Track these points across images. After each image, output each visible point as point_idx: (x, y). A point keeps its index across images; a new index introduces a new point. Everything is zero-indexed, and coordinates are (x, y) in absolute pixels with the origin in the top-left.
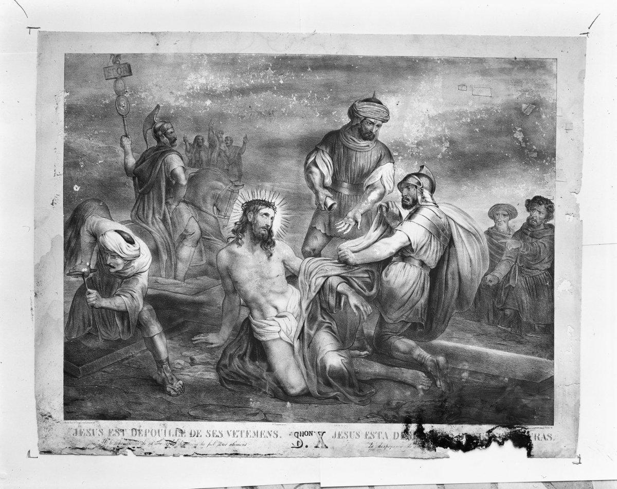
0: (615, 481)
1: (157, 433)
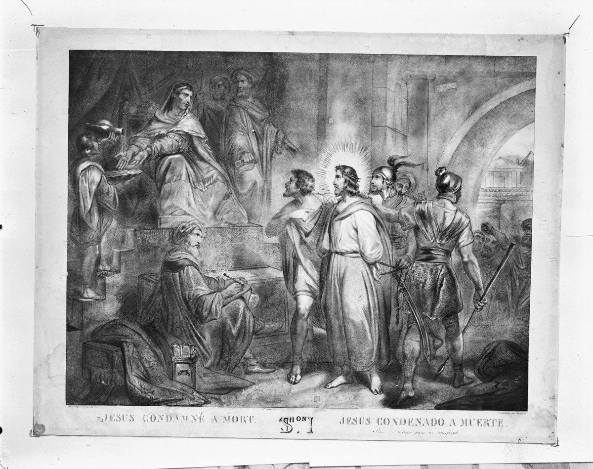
0: (591, 464)
1: (437, 423)
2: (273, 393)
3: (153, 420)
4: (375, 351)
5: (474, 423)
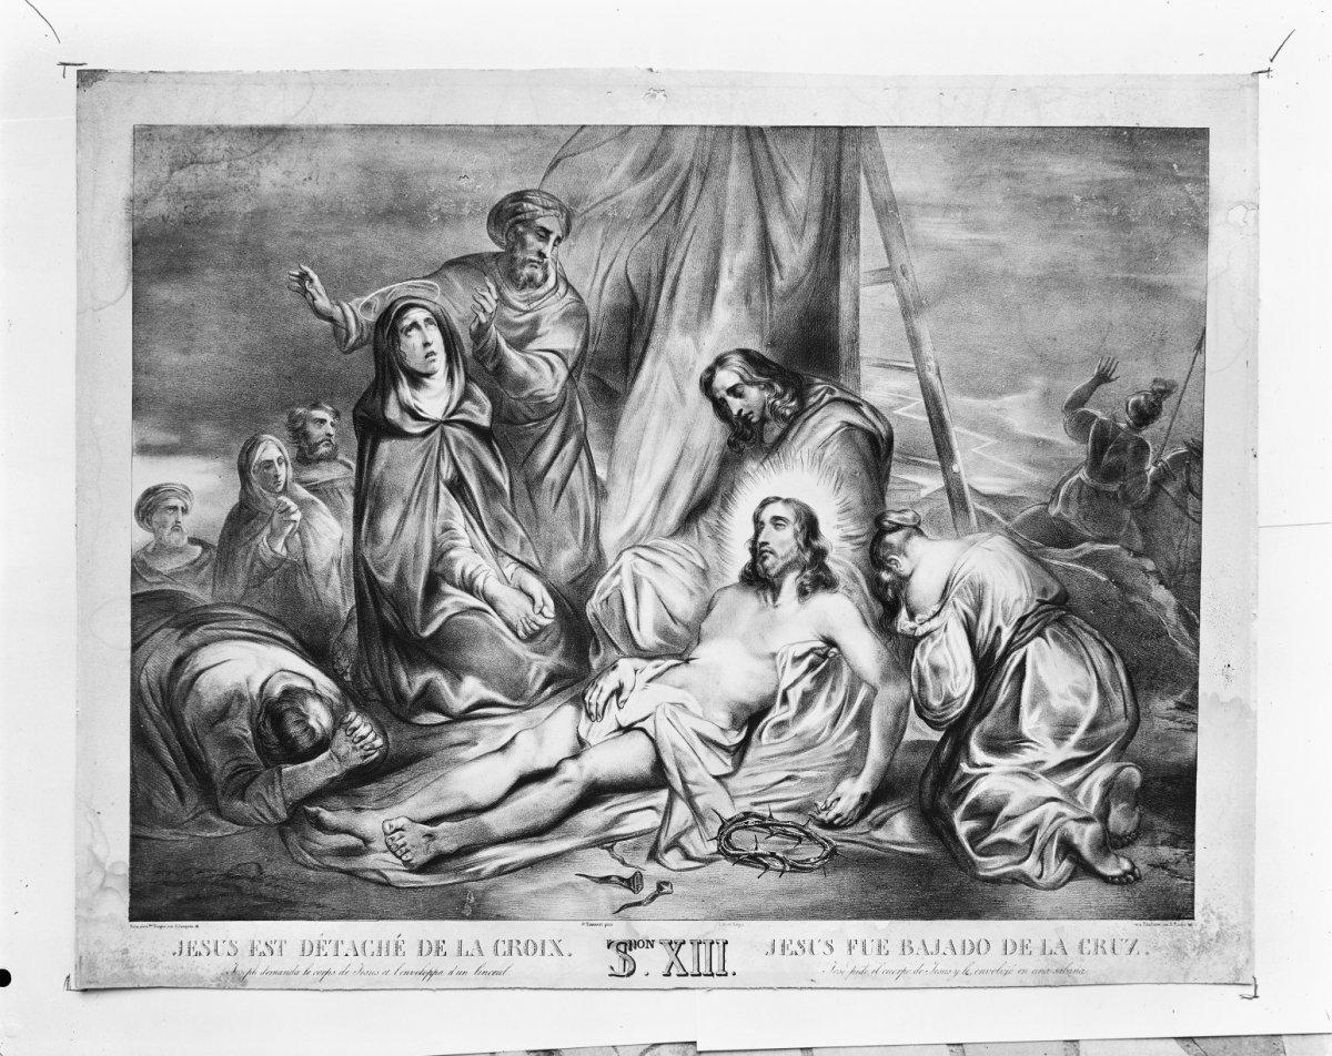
2: (991, 794)
5: (488, 947)
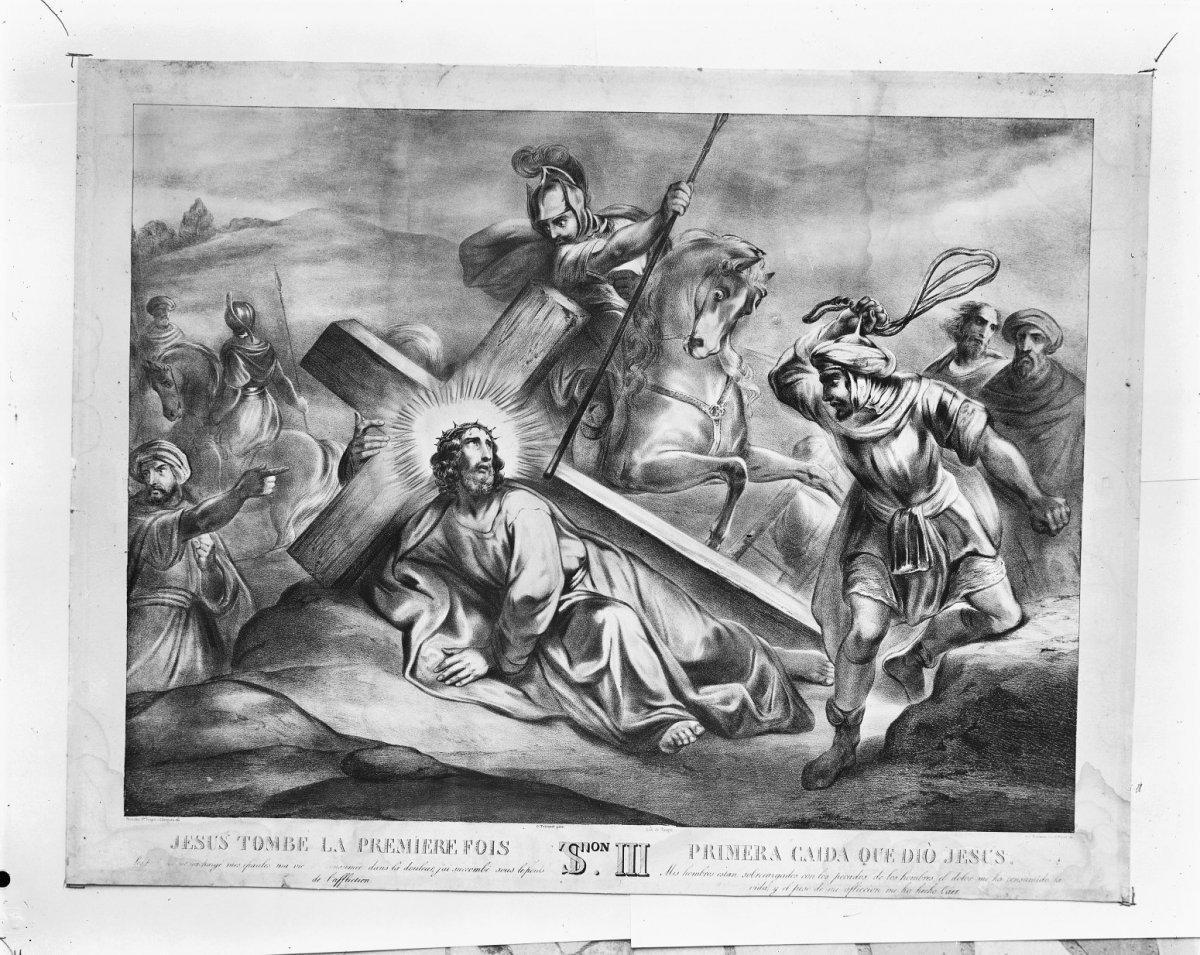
3: (481, 851)
4: (743, 627)
